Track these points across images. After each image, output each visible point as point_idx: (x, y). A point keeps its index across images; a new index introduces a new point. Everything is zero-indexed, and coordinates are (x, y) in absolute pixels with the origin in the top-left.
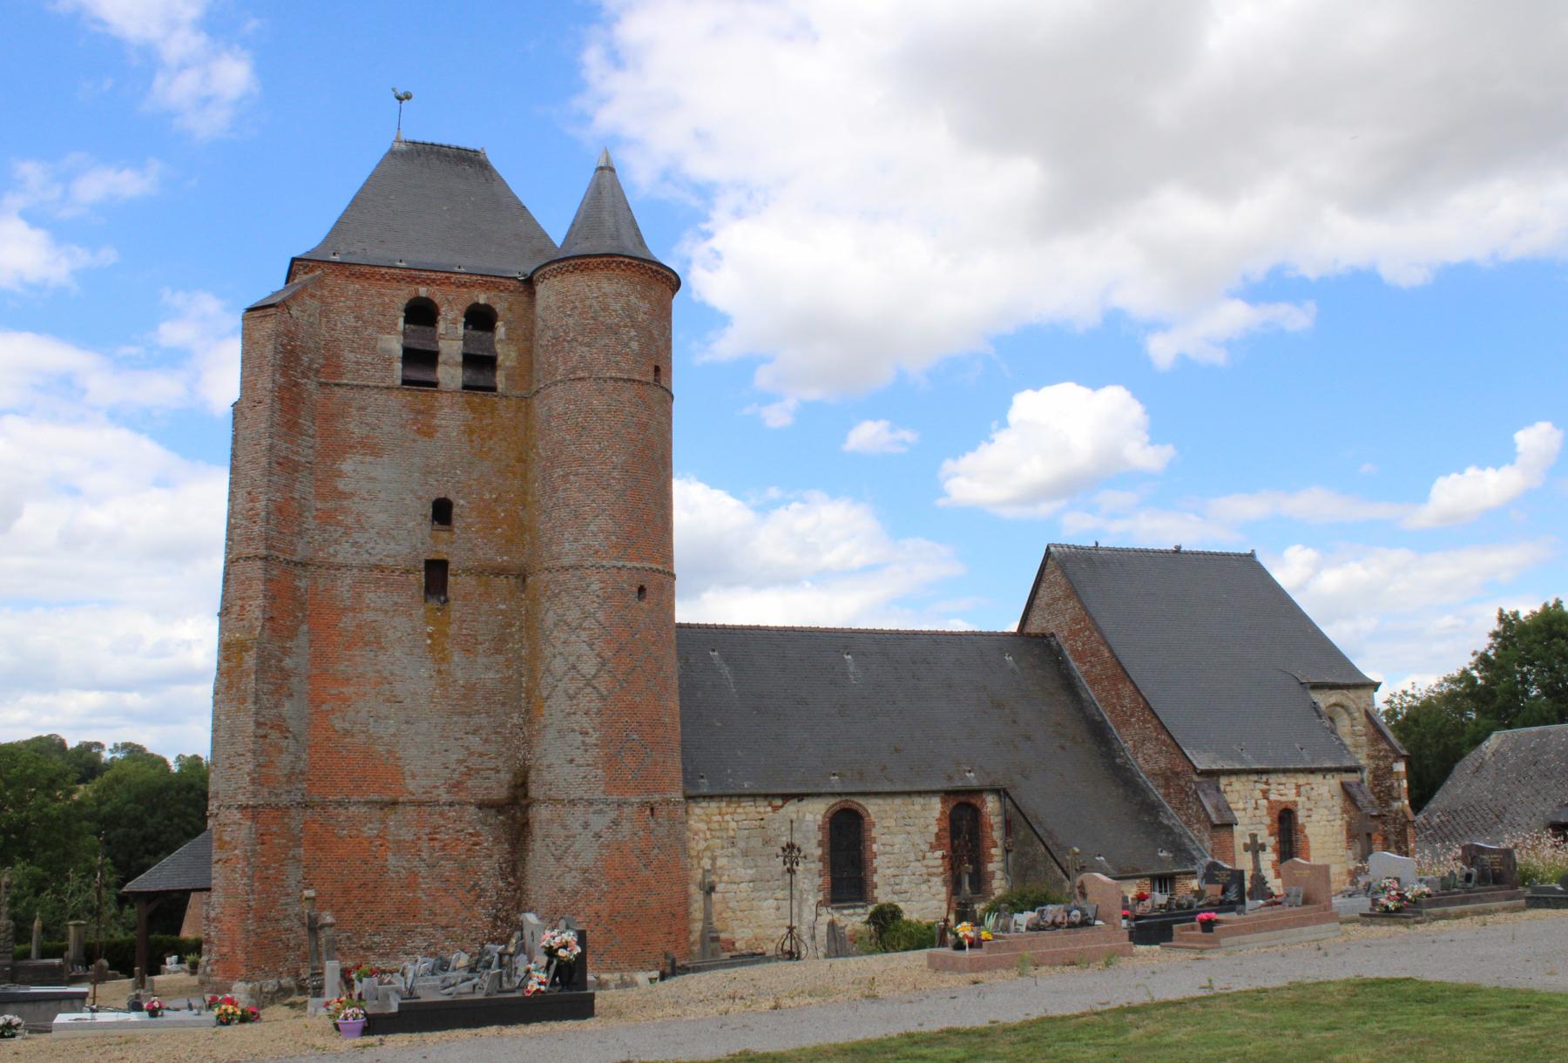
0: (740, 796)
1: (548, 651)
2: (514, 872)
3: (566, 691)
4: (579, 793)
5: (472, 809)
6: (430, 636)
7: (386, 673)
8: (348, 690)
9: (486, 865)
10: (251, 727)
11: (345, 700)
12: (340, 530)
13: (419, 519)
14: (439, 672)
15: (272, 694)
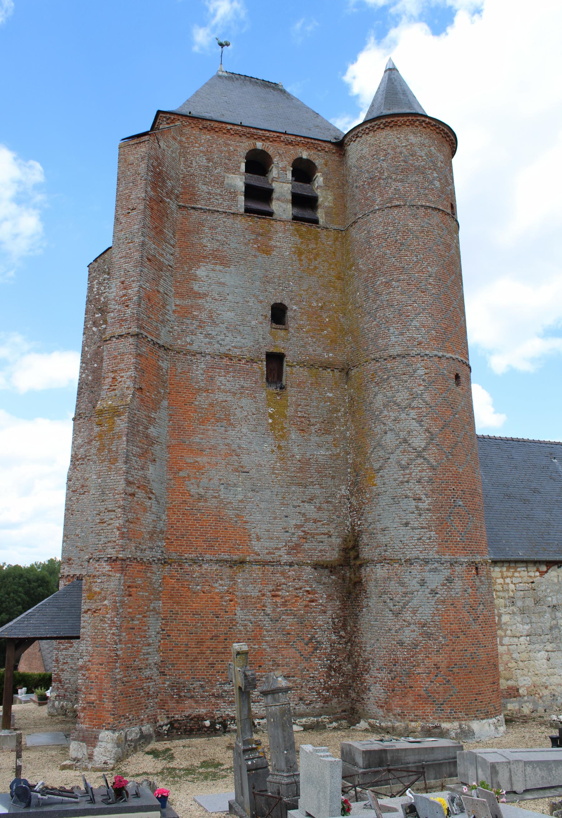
0: (516, 562)
1: (379, 429)
3: (398, 463)
5: (309, 569)
6: (271, 416)
7: (234, 447)
8: (202, 460)
9: (321, 619)
10: (121, 485)
12: (196, 323)
13: (261, 318)
14: (279, 447)
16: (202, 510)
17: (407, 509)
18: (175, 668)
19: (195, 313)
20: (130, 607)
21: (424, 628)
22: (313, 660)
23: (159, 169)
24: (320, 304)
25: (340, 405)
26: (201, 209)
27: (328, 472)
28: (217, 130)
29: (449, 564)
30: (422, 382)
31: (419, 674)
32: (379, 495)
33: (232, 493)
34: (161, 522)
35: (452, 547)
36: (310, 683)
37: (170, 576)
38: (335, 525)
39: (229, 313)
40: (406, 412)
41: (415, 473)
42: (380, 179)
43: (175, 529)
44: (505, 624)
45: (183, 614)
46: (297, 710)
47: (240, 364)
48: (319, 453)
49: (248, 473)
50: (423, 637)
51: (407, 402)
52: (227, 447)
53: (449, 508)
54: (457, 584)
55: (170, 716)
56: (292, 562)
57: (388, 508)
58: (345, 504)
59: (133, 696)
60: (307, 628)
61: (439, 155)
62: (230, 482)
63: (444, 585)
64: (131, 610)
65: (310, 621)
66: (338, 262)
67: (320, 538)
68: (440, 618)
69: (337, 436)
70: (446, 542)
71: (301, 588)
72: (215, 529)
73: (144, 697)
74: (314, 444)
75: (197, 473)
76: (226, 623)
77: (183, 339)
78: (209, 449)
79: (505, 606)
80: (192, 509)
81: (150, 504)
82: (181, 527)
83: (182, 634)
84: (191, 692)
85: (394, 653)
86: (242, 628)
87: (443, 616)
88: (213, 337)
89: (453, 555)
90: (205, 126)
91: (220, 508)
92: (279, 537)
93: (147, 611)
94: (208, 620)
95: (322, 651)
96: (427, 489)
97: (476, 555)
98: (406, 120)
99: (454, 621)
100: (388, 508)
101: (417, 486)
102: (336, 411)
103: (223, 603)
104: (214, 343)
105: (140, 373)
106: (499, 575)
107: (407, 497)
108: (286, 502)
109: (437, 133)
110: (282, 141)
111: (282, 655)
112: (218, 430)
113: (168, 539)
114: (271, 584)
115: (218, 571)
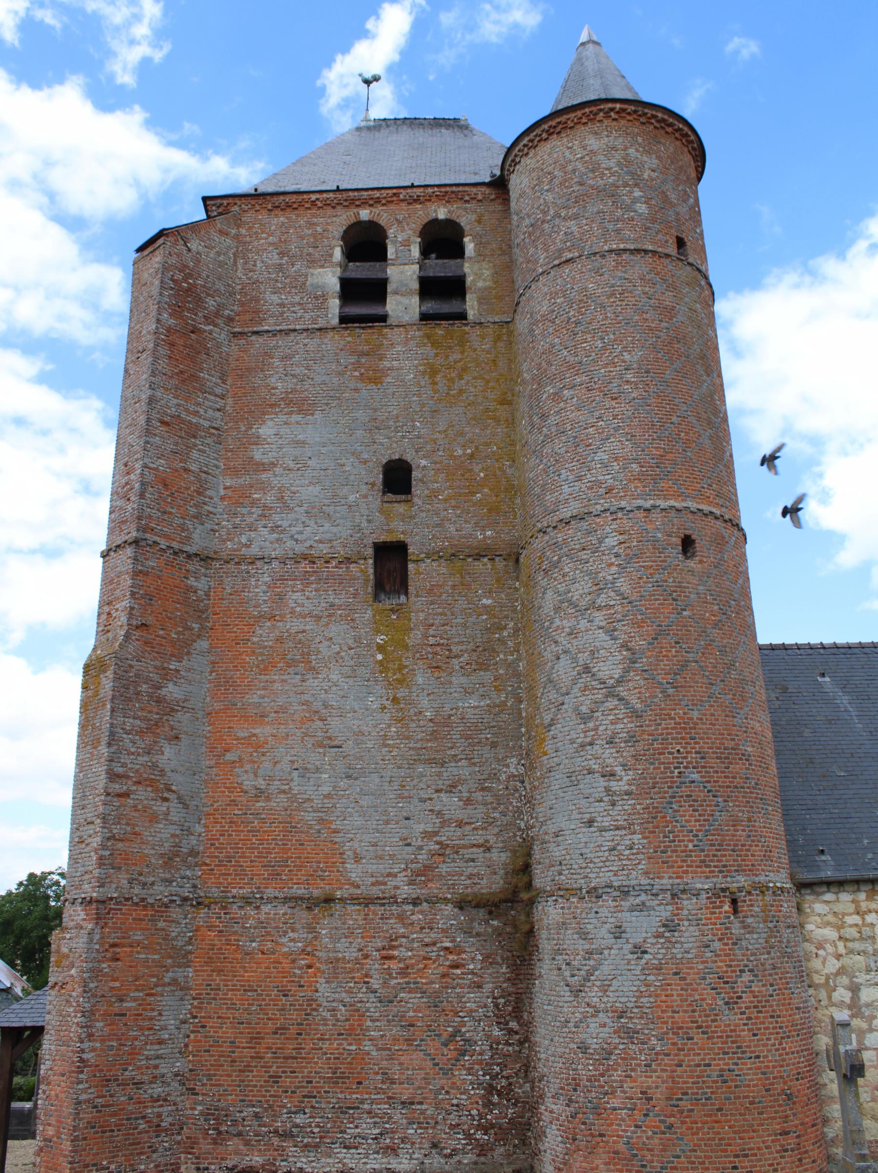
2: (517, 1012)
3: (576, 709)
4: (606, 877)
5: (448, 909)
6: (381, 648)
7: (317, 705)
8: (263, 731)
9: (472, 1001)
11: (258, 746)
12: (257, 511)
13: (364, 489)
14: (395, 700)
15: (141, 733)
16: (261, 814)
17: (590, 794)
18: (213, 1082)
19: (255, 496)
20: (115, 980)
21: (622, 1020)
22: (457, 1073)
23: (188, 283)
24: (469, 451)
25: (506, 617)
26: (268, 331)
27: (483, 736)
28: (295, 206)
29: (668, 896)
30: (613, 560)
31: (615, 1109)
32: (550, 771)
33: (312, 783)
34: (192, 837)
35: (676, 862)
36: (451, 1116)
37: (207, 926)
38: (497, 830)
39: (311, 488)
40: (587, 617)
41: (604, 727)
42: (543, 222)
43: (217, 848)
44: (868, 1005)
45: (228, 990)
46: (427, 1166)
47: (328, 567)
48: (467, 705)
49: (341, 747)
50: (619, 1037)
51: (589, 598)
52: (304, 707)
53: (669, 787)
54: (686, 934)
55: (201, 1166)
56: (418, 898)
57: (562, 795)
58: (516, 790)
59: (119, 1130)
60: (447, 1015)
61: (645, 159)
62: (309, 766)
63: (658, 936)
64: (117, 984)
65: (451, 1002)
66: (501, 375)
67: (468, 853)
68: (652, 1000)
69: (501, 672)
70: (662, 852)
71: (434, 944)
72: (283, 844)
73: (147, 1132)
74: (458, 690)
75: (255, 754)
76: (299, 1005)
77: (236, 539)
78: (275, 712)
79: (868, 970)
80: (246, 814)
81: (165, 809)
82: (227, 844)
83: (225, 1023)
84: (238, 1125)
85: (574, 1066)
86: (328, 1015)
87: (657, 996)
88: (285, 530)
89: (677, 878)
90: (277, 204)
91: (291, 810)
92: (394, 855)
93: (156, 985)
94: (270, 1000)
95: (474, 1058)
96: (624, 754)
97: (733, 874)
98: (580, 115)
99: (681, 1006)
100: (562, 795)
101: (608, 751)
102: (498, 628)
103: (296, 971)
104: (285, 539)
105: (142, 602)
106: (851, 908)
107: (590, 772)
108: (406, 794)
109: (643, 124)
110: (402, 200)
111: (400, 1064)
112: (289, 681)
113: (207, 865)
114: (379, 937)
115: (287, 917)
